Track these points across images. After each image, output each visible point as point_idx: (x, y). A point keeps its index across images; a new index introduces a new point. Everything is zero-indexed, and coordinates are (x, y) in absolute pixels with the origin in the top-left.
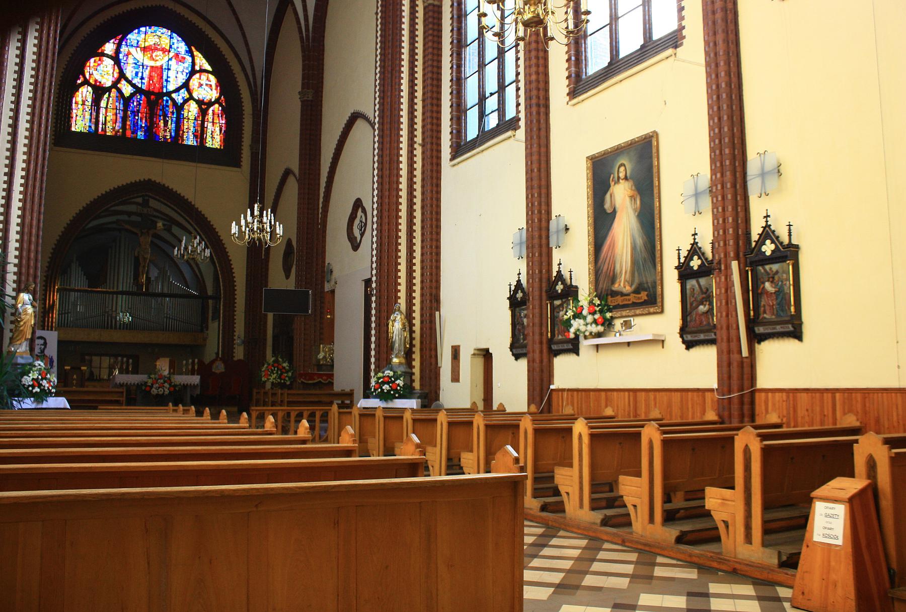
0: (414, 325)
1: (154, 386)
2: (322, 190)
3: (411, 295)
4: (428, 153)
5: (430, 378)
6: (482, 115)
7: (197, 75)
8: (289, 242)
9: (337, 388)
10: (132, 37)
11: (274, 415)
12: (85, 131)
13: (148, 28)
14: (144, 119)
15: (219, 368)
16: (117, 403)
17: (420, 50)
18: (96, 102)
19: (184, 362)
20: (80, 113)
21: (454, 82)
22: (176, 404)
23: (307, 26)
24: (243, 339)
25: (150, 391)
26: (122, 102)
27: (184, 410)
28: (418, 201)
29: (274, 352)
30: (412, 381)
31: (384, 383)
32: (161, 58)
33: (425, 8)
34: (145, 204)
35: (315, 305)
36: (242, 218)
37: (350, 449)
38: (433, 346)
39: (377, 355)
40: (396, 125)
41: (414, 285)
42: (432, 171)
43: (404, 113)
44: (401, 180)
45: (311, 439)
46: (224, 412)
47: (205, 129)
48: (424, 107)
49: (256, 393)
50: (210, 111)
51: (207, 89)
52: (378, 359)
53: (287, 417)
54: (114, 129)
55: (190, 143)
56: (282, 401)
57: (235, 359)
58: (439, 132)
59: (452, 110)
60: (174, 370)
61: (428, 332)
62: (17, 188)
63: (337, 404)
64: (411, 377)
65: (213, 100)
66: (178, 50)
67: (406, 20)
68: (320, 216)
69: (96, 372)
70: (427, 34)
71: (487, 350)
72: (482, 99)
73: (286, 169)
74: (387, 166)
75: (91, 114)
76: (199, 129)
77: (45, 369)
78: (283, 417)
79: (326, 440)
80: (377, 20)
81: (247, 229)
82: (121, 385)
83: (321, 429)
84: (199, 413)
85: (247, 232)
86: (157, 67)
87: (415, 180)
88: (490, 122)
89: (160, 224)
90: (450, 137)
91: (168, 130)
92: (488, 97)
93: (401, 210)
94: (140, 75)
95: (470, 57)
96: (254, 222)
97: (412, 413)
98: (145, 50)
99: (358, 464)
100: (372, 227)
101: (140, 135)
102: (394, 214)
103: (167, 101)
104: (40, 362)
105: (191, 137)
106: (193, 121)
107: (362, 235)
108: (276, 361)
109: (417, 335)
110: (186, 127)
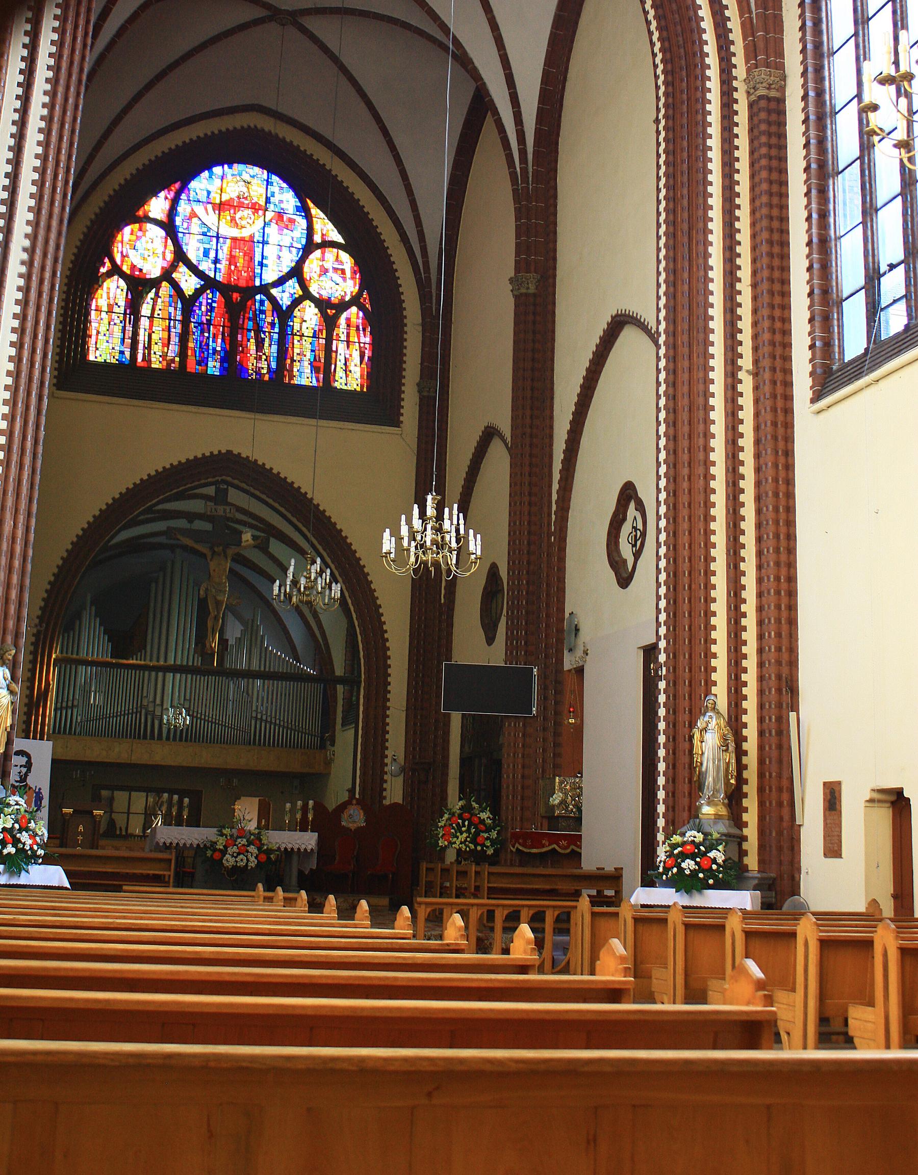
0: (745, 739)
1: (230, 850)
2: (557, 466)
3: (737, 677)
4: (767, 389)
5: (780, 849)
6: (874, 309)
7: (318, 253)
8: (493, 572)
9: (589, 864)
10: (200, 185)
11: (465, 915)
12: (114, 361)
13: (226, 166)
14: (220, 336)
15: (355, 819)
16: (157, 880)
17: (743, 187)
18: (133, 307)
19: (288, 805)
20: (103, 329)
21: (815, 246)
22: (270, 888)
23: (523, 152)
24: (403, 763)
25: (222, 859)
26: (179, 305)
27: (285, 899)
28: (748, 484)
29: (462, 790)
30: (743, 853)
31: (684, 856)
32: (251, 222)
33: (751, 106)
34: (221, 498)
35: (544, 698)
36: (403, 522)
37: (617, 986)
38: (785, 783)
39: (671, 799)
40: (701, 336)
41: (745, 657)
42: (775, 424)
43: (717, 312)
44: (713, 443)
45: (537, 963)
46: (364, 904)
47: (334, 355)
48: (755, 298)
49: (427, 869)
50: (342, 321)
51: (337, 278)
52: (671, 808)
53: (488, 921)
54: (165, 356)
55: (305, 381)
56: (477, 888)
57: (387, 802)
58: (787, 346)
59: (813, 355)
60: (267, 821)
61: (774, 753)
62: (28, 176)
63: (589, 896)
64: (740, 845)
65: (347, 298)
66: (282, 206)
67: (715, 129)
68: (553, 517)
69: (120, 820)
70: (756, 155)
71: (899, 793)
72: (873, 277)
73: (487, 428)
74: (684, 416)
75: (124, 327)
76: (322, 355)
77: (26, 811)
78: (480, 919)
79: (565, 970)
80: (658, 133)
81: (413, 544)
82: (167, 847)
83: (556, 946)
84: (316, 907)
85: (413, 549)
86: (243, 239)
87: (741, 442)
88: (891, 323)
89: (247, 537)
90: (809, 354)
91: (264, 357)
92: (885, 273)
93: (714, 505)
94: (212, 255)
95: (844, 196)
96: (425, 530)
97: (744, 918)
98: (221, 207)
99: (636, 1017)
100: (658, 539)
101: (213, 367)
102: (701, 512)
103: (262, 302)
104: (17, 798)
105: (307, 370)
106: (310, 340)
107: (637, 555)
108: (467, 808)
109: (751, 760)
110: (297, 351)
